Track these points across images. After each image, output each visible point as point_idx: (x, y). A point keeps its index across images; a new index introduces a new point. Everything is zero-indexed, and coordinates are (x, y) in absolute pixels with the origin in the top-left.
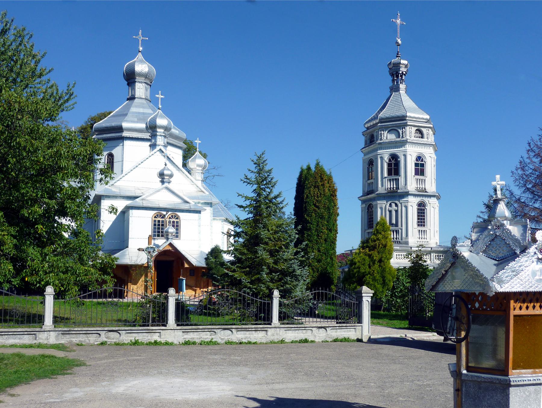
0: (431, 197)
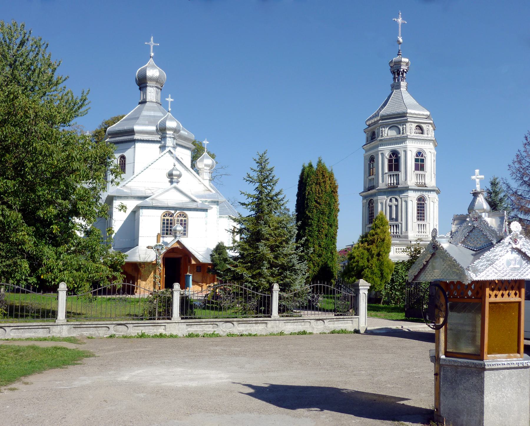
0: (430, 192)
